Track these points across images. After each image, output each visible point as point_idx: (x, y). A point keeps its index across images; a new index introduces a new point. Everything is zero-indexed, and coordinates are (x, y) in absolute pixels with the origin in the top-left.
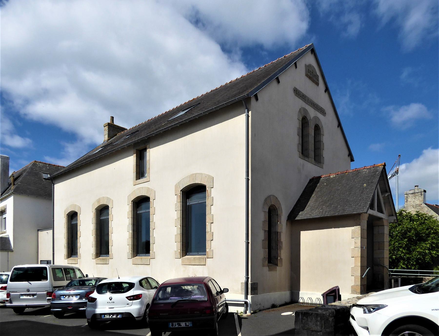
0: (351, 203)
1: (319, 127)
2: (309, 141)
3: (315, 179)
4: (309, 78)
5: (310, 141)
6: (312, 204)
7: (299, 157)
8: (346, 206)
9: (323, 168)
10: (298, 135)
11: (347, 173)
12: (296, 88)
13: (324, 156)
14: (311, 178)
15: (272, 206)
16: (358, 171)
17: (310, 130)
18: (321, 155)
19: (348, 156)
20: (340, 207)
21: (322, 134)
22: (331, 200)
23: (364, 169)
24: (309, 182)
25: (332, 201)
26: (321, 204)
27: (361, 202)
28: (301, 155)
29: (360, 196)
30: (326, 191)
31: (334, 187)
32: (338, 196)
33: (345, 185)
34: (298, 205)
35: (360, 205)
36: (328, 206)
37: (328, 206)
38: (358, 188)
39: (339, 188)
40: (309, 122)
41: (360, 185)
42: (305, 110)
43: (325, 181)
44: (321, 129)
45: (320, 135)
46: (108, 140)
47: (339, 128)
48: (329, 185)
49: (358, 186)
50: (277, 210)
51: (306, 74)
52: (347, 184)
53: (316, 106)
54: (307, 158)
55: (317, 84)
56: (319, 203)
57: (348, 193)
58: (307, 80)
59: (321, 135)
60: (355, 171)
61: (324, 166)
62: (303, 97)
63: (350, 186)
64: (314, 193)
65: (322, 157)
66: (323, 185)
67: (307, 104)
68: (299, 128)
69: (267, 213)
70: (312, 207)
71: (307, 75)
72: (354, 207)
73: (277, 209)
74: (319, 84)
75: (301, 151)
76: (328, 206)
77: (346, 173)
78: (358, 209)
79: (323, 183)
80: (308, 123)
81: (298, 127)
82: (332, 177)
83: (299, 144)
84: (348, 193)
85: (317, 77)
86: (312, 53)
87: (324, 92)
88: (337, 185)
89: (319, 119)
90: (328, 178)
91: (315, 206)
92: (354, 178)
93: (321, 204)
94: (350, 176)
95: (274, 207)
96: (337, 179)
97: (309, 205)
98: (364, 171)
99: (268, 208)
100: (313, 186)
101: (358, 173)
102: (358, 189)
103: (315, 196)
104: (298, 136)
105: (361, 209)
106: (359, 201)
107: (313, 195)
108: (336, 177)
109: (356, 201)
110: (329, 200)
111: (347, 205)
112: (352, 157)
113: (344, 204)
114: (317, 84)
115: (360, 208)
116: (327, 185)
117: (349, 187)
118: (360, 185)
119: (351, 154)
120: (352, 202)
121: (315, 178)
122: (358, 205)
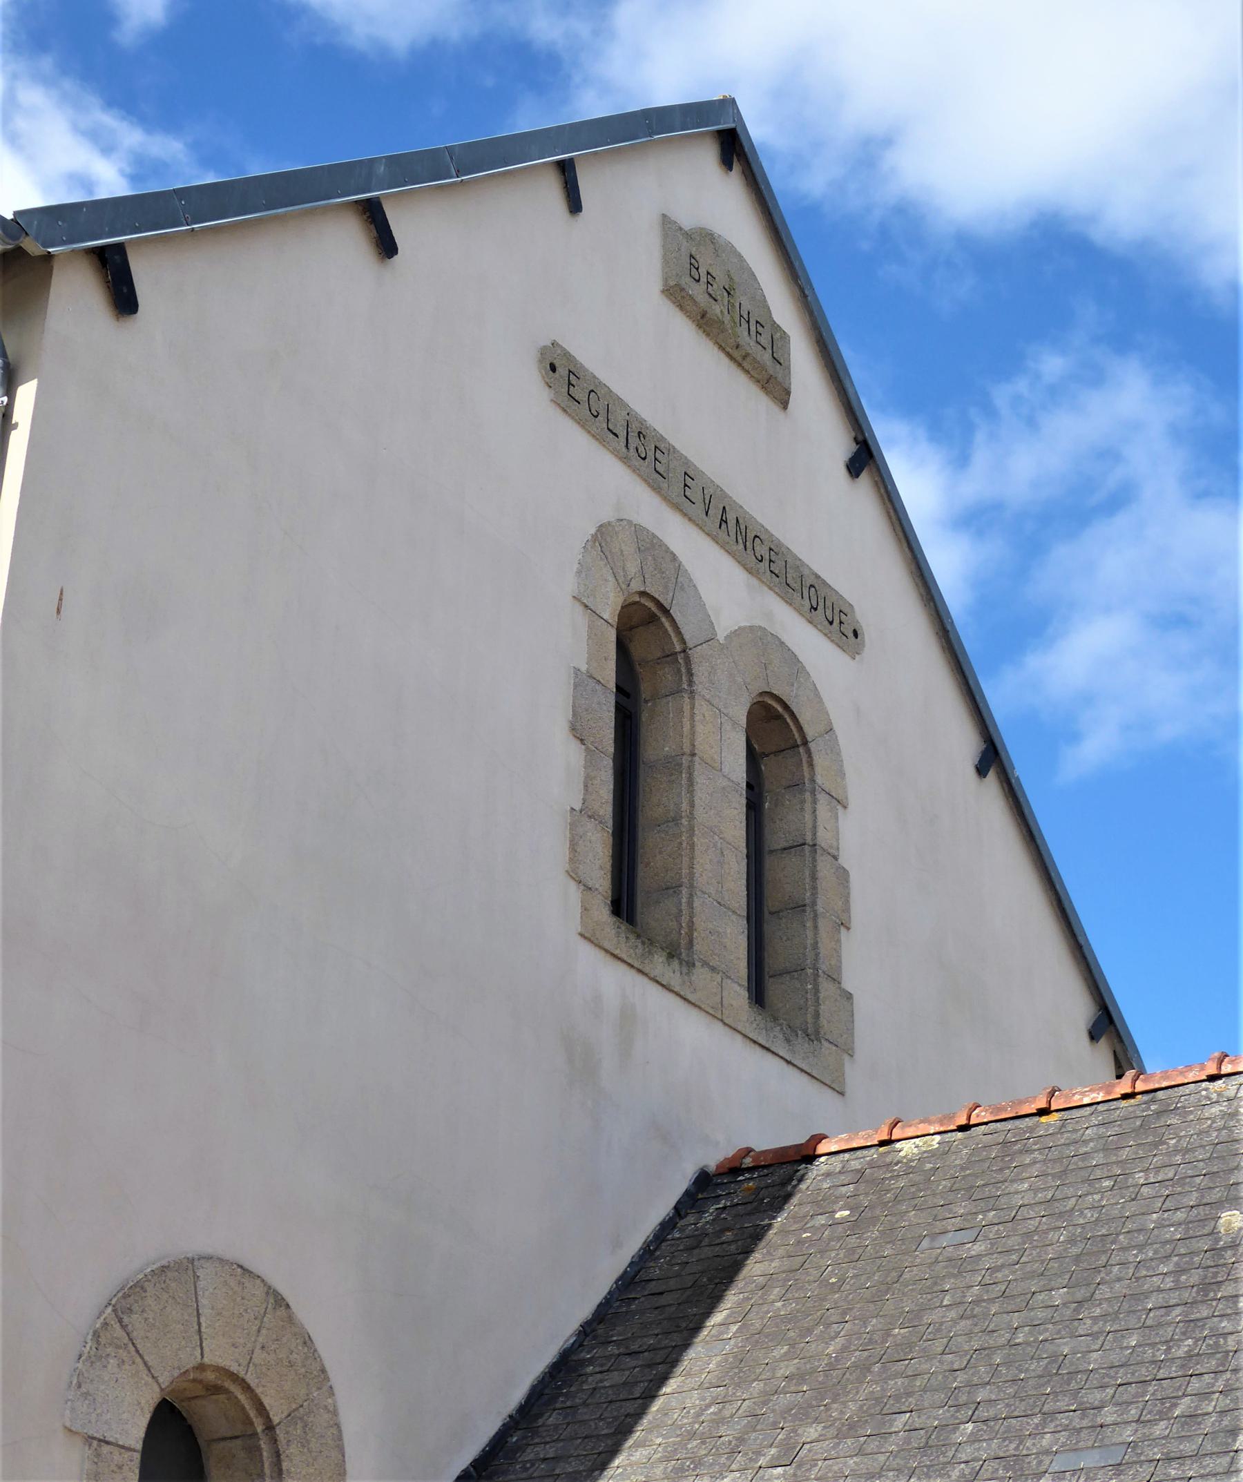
0: (1096, 1397)
1: (800, 729)
2: (691, 817)
3: (750, 1169)
4: (699, 326)
5: (699, 812)
6: (694, 1400)
7: (581, 935)
8: (1044, 1423)
9: (842, 1094)
10: (578, 732)
11: (1056, 1116)
12: (567, 355)
13: (848, 984)
14: (712, 1159)
15: (215, 1389)
16: (1160, 1094)
17: (699, 728)
18: (823, 967)
19: (1093, 1036)
20: (974, 1439)
21: (827, 787)
22: (884, 1369)
23: (1212, 1078)
24: (687, 1193)
25: (896, 1375)
26: (784, 1400)
27: (1195, 1384)
28: (602, 912)
29: (1191, 1324)
30: (842, 1281)
31: (925, 1243)
32: (963, 1323)
33: (1035, 1222)
34: (553, 1419)
35: (1192, 1417)
36: (852, 1427)
37: (851, 1428)
38: (1162, 1253)
39: (978, 1248)
40: (695, 654)
41: (1180, 1215)
42: (650, 546)
43: (844, 1189)
44: (812, 746)
45: (808, 795)
46: (177, 1377)
47: (992, 776)
48: (874, 1220)
49: (1160, 1225)
50: (274, 1441)
51: (666, 280)
52: (1059, 1207)
53: (762, 550)
54: (676, 963)
55: (781, 397)
56: (766, 1397)
57: (1058, 1296)
58: (682, 329)
59: (822, 799)
60: (1125, 1097)
61: (854, 1074)
62: (634, 441)
63: (1083, 1226)
64: (732, 1299)
65: (826, 988)
66: (822, 1220)
67: (677, 507)
68: (591, 677)
69: (117, 1456)
70: (692, 1435)
71: (675, 293)
72: (1128, 1434)
73: (270, 1428)
74: (788, 393)
75: (602, 881)
76: (851, 1428)
77: (1044, 1119)
78: (1169, 1459)
79: (823, 1205)
80: (688, 661)
81: (577, 671)
82: (907, 1149)
83: (586, 812)
84: (1058, 1296)
85: (776, 341)
86: (727, 163)
87: (843, 471)
88: (951, 1224)
89: (793, 660)
90: (872, 1165)
91: (719, 1421)
92: (1124, 1154)
93: (784, 1400)
94: (1085, 1142)
95: (242, 1397)
96: (963, 1169)
97: (665, 1412)
98: (1219, 1094)
99: (149, 1399)
100: (729, 1235)
101: (1159, 1114)
102: (1168, 1257)
103: (734, 1328)
104: (575, 745)
105: (1197, 1456)
106: (1174, 1370)
107: (717, 1318)
108: (944, 1152)
109: (1143, 1372)
110: (865, 1368)
111: (1049, 1416)
112: (1125, 1051)
113: (1021, 1408)
114: (781, 397)
115: (1188, 1447)
116: (856, 1225)
117: (1072, 1241)
118: (1180, 1215)
119: (1111, 1021)
120: (1103, 1387)
121: (748, 1162)
122: (1163, 1415)
